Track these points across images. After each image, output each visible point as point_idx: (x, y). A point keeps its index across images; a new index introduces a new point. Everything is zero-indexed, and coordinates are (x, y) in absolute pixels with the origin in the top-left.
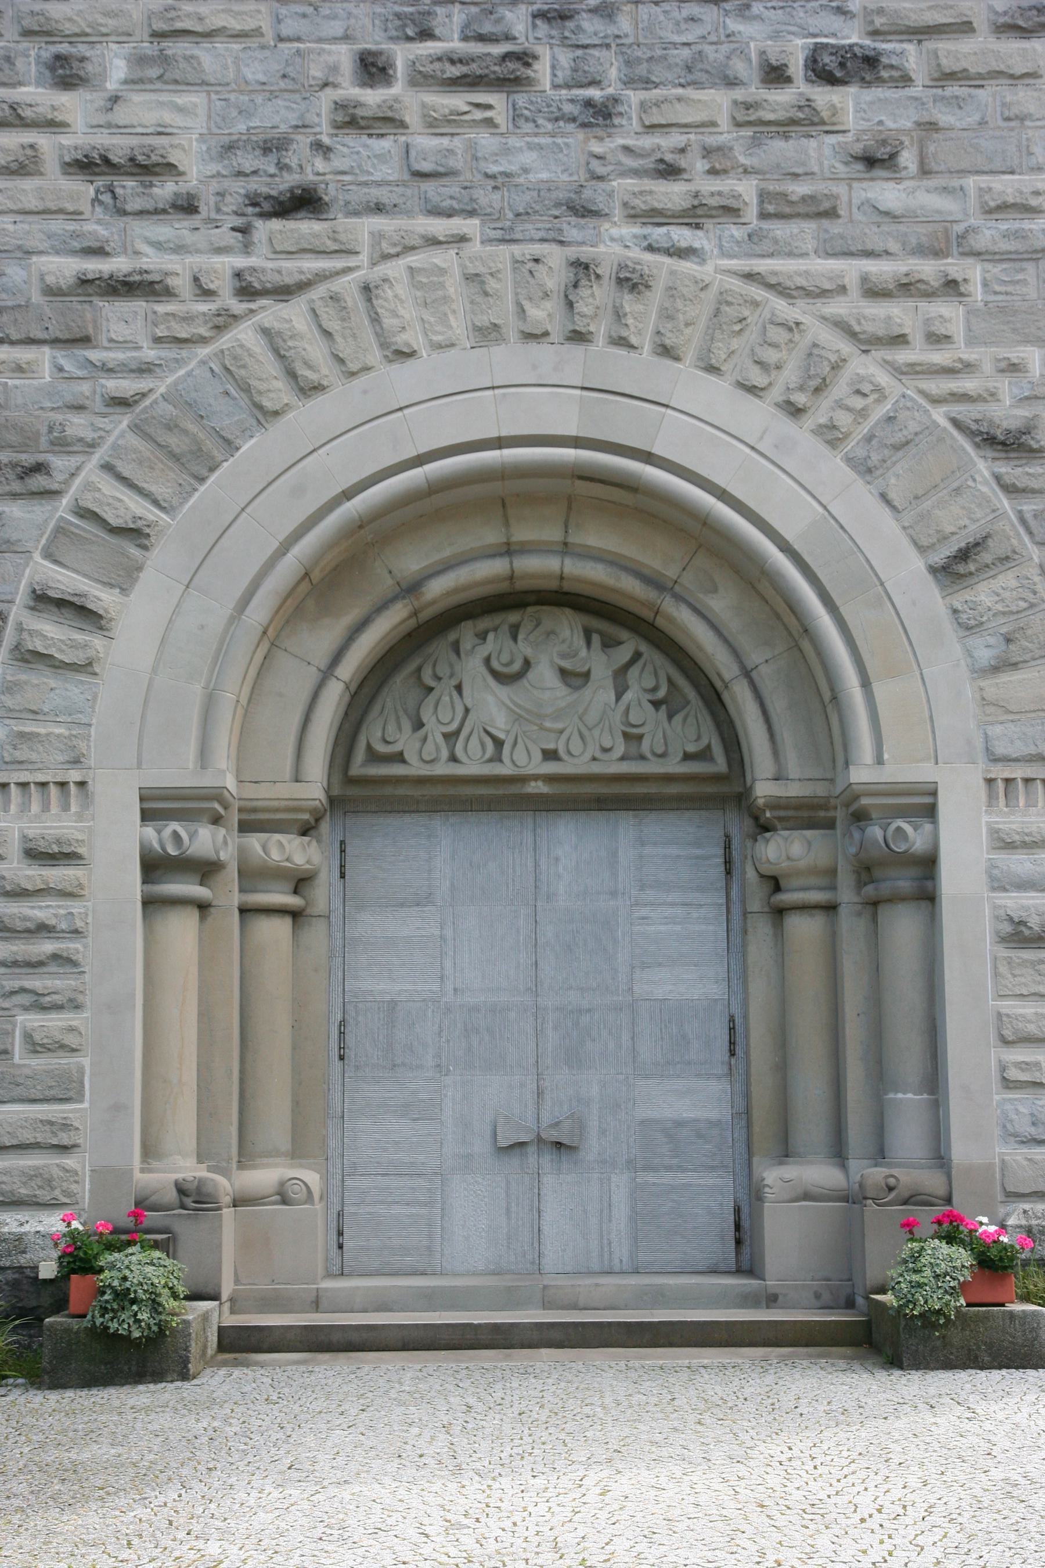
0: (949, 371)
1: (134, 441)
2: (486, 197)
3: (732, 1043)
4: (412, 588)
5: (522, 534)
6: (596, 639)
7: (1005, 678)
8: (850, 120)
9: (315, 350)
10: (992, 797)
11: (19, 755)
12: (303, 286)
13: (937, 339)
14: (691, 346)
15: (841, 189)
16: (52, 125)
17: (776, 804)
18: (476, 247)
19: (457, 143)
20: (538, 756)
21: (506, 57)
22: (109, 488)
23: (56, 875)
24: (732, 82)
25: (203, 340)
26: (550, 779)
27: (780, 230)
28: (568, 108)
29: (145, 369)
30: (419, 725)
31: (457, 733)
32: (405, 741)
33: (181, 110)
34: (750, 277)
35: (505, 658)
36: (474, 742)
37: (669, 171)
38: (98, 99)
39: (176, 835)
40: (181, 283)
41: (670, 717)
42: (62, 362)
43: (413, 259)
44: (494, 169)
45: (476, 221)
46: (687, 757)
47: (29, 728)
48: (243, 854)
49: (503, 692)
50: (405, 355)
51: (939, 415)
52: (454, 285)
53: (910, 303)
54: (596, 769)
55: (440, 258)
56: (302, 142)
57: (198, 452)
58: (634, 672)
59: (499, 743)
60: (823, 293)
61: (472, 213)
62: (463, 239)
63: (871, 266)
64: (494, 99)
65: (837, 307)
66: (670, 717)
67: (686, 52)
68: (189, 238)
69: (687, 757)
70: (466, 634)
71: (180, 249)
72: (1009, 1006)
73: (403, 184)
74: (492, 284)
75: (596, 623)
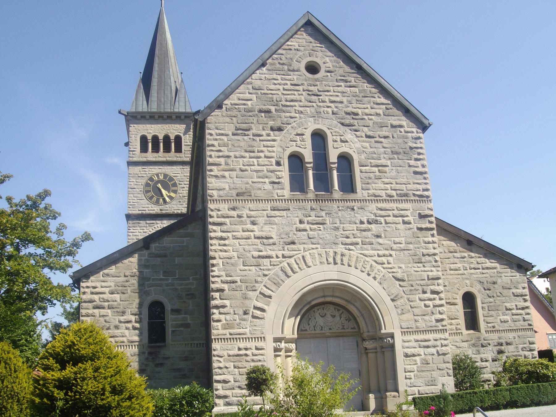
0: (391, 268)
1: (268, 281)
2: (321, 241)
3: (360, 374)
4: (310, 302)
5: (326, 294)
6: (336, 310)
7: (403, 315)
8: (374, 229)
9: (295, 266)
10: (402, 335)
11: (254, 333)
12: (293, 256)
13: (389, 263)
14: (353, 265)
15: (373, 240)
16: (252, 231)
17: (368, 336)
18: (319, 249)
19: (316, 233)
20: (328, 329)
21: (322, 220)
22: (264, 288)
23: (260, 352)
24: (356, 224)
25: (278, 265)
26: (330, 333)
27: (365, 246)
28: (332, 227)
29: (269, 270)
30: (309, 324)
31: (315, 326)
32: (307, 327)
33: (272, 228)
34: (361, 254)
35: (322, 313)
36: (318, 328)
37: (348, 237)
38: (260, 227)
39: (279, 345)
40: (274, 256)
41: (349, 322)
42: (257, 269)
43: (310, 251)
44: (321, 237)
45: (319, 245)
46: (352, 328)
47: (255, 328)
48: (285, 347)
49: (321, 319)
50: (309, 267)
51: (390, 275)
52: (317, 256)
53: (385, 257)
54: (338, 331)
55: (314, 251)
56: (292, 233)
57: (279, 283)
58: (342, 315)
59: (322, 327)
60: (372, 256)
61: (318, 244)
62: (317, 248)
63: (379, 252)
64: (321, 226)
65: (374, 258)
66: (349, 322)
67: (349, 219)
68: (275, 249)
69: (352, 328)
70: (316, 309)
71: (274, 250)
72: (406, 366)
73: (307, 239)
74: (322, 255)
75: (335, 307)
